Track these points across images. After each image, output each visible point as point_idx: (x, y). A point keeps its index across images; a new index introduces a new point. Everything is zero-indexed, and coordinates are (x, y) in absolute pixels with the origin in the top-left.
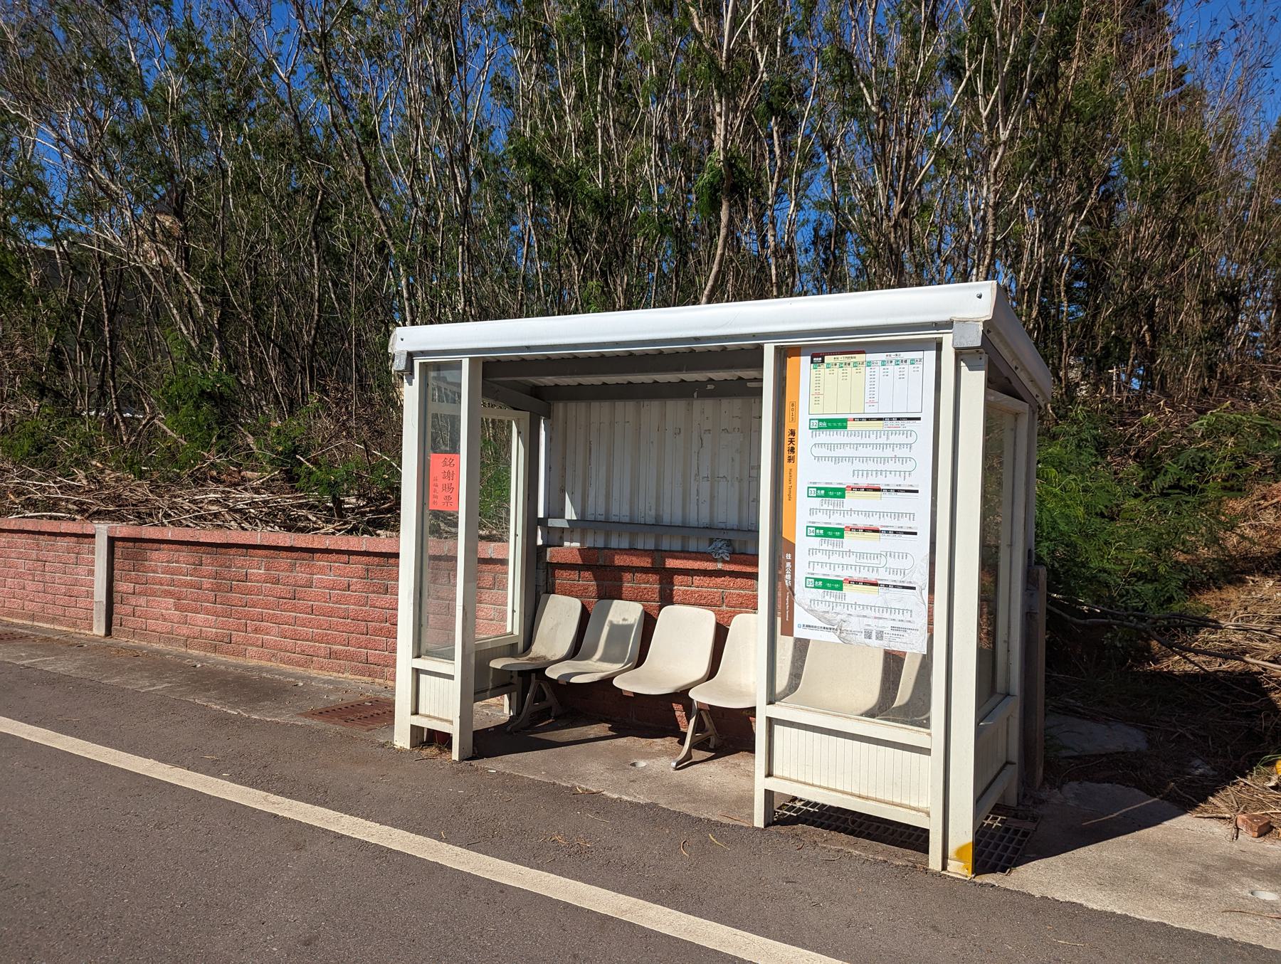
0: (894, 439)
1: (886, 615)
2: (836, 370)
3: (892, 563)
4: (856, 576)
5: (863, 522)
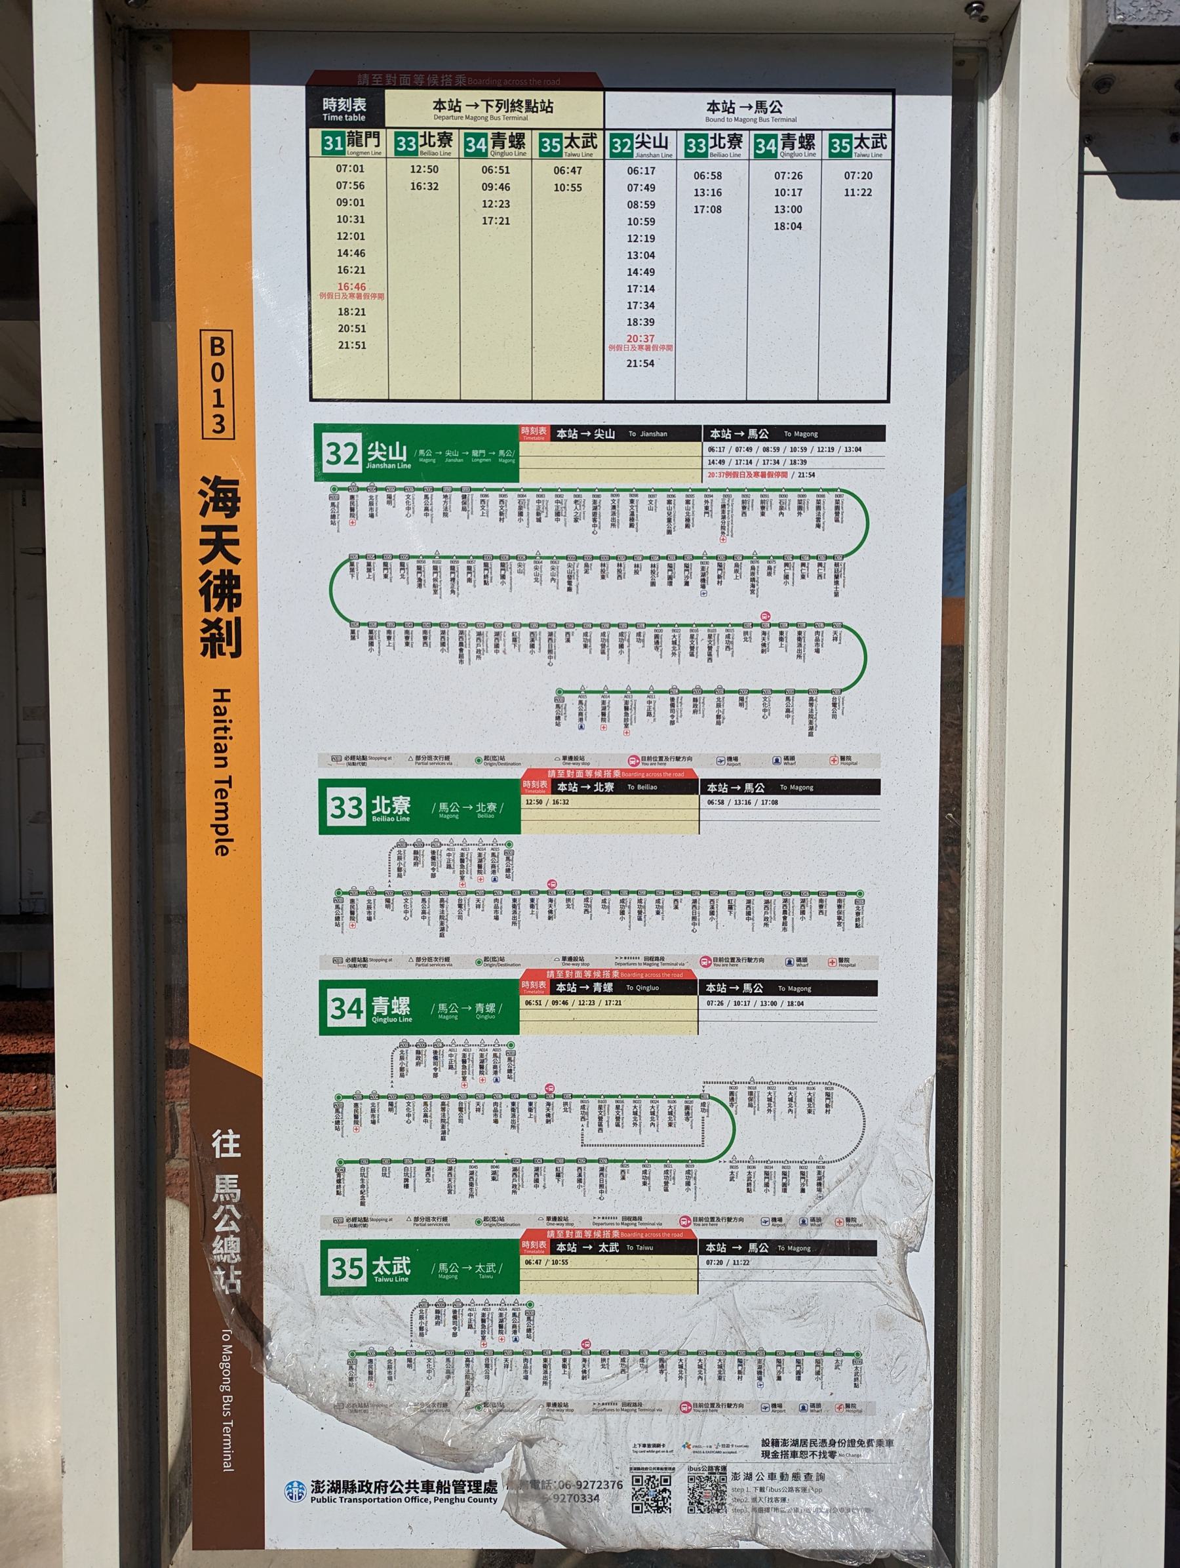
0: (757, 533)
1: (738, 1389)
2: (456, 171)
3: (766, 1136)
4: (584, 1210)
5: (608, 943)
